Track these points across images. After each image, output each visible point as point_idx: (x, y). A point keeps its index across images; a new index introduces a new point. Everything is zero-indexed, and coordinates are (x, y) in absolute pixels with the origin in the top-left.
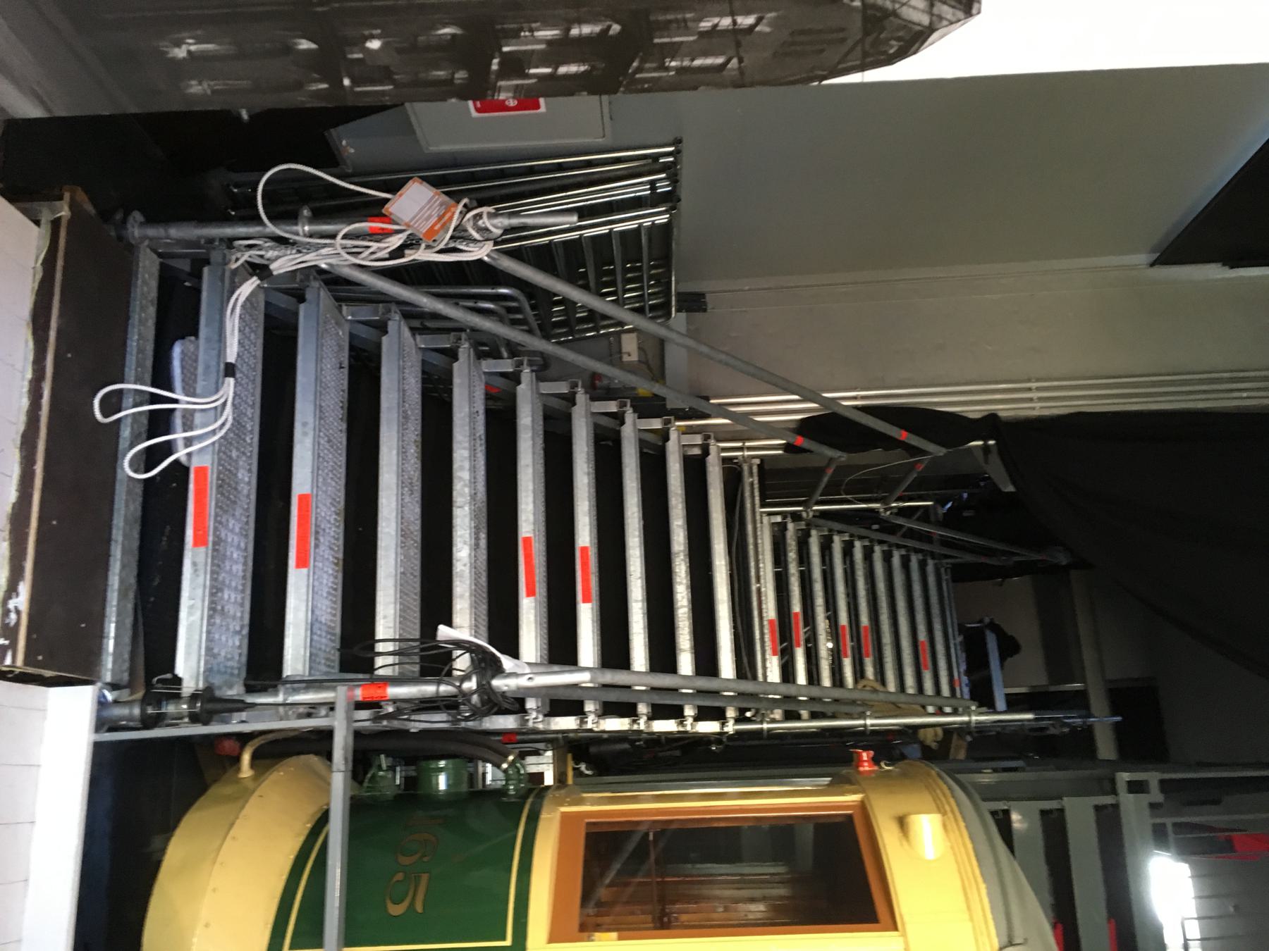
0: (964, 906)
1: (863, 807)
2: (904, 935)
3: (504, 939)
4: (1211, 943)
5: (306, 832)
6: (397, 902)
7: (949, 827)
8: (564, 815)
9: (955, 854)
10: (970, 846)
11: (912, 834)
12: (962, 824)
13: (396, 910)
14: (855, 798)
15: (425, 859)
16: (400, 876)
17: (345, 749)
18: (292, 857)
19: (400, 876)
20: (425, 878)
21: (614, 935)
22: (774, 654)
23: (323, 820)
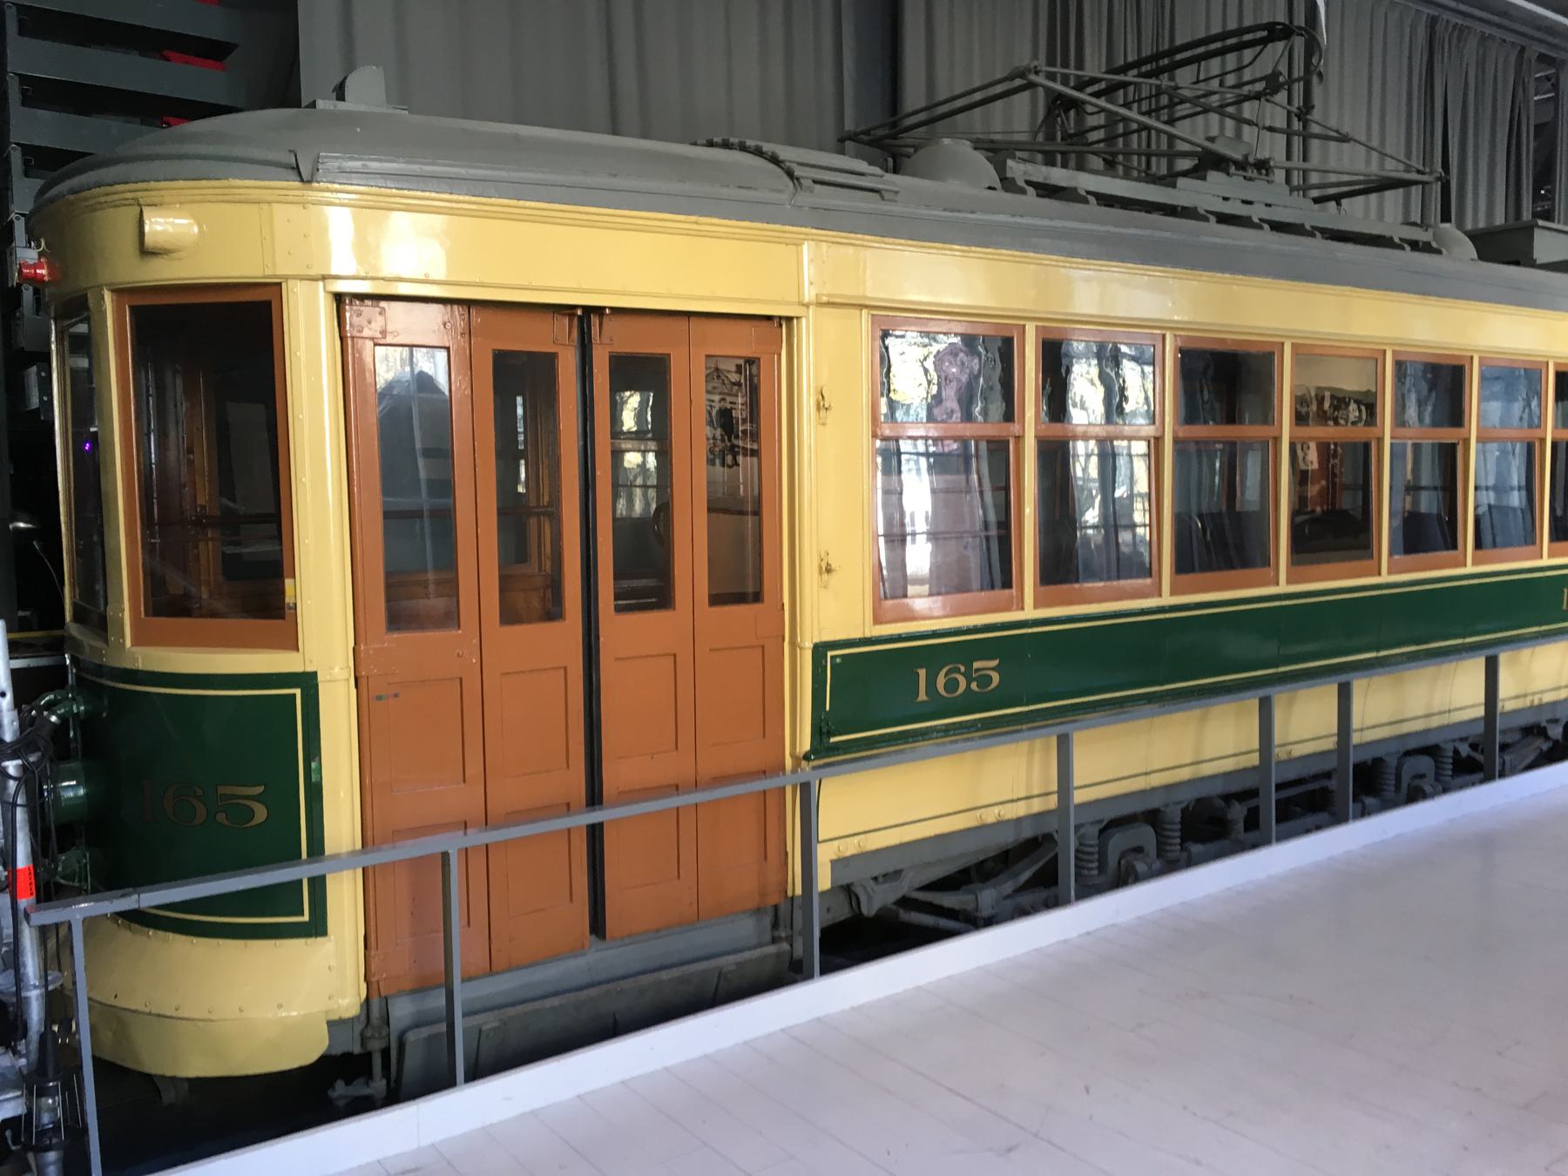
0: (255, 207)
1: (120, 292)
2: (287, 278)
3: (294, 695)
4: (941, 495)
5: (161, 933)
6: (251, 814)
7: (155, 200)
8: (135, 643)
9: (193, 202)
10: (181, 183)
11: (167, 246)
12: (153, 184)
13: (261, 814)
14: (108, 296)
15: (199, 792)
16: (221, 817)
17: (110, 899)
18: (195, 940)
19: (221, 817)
20: (222, 790)
21: (288, 582)
22: (1469, 756)
23: (137, 918)
